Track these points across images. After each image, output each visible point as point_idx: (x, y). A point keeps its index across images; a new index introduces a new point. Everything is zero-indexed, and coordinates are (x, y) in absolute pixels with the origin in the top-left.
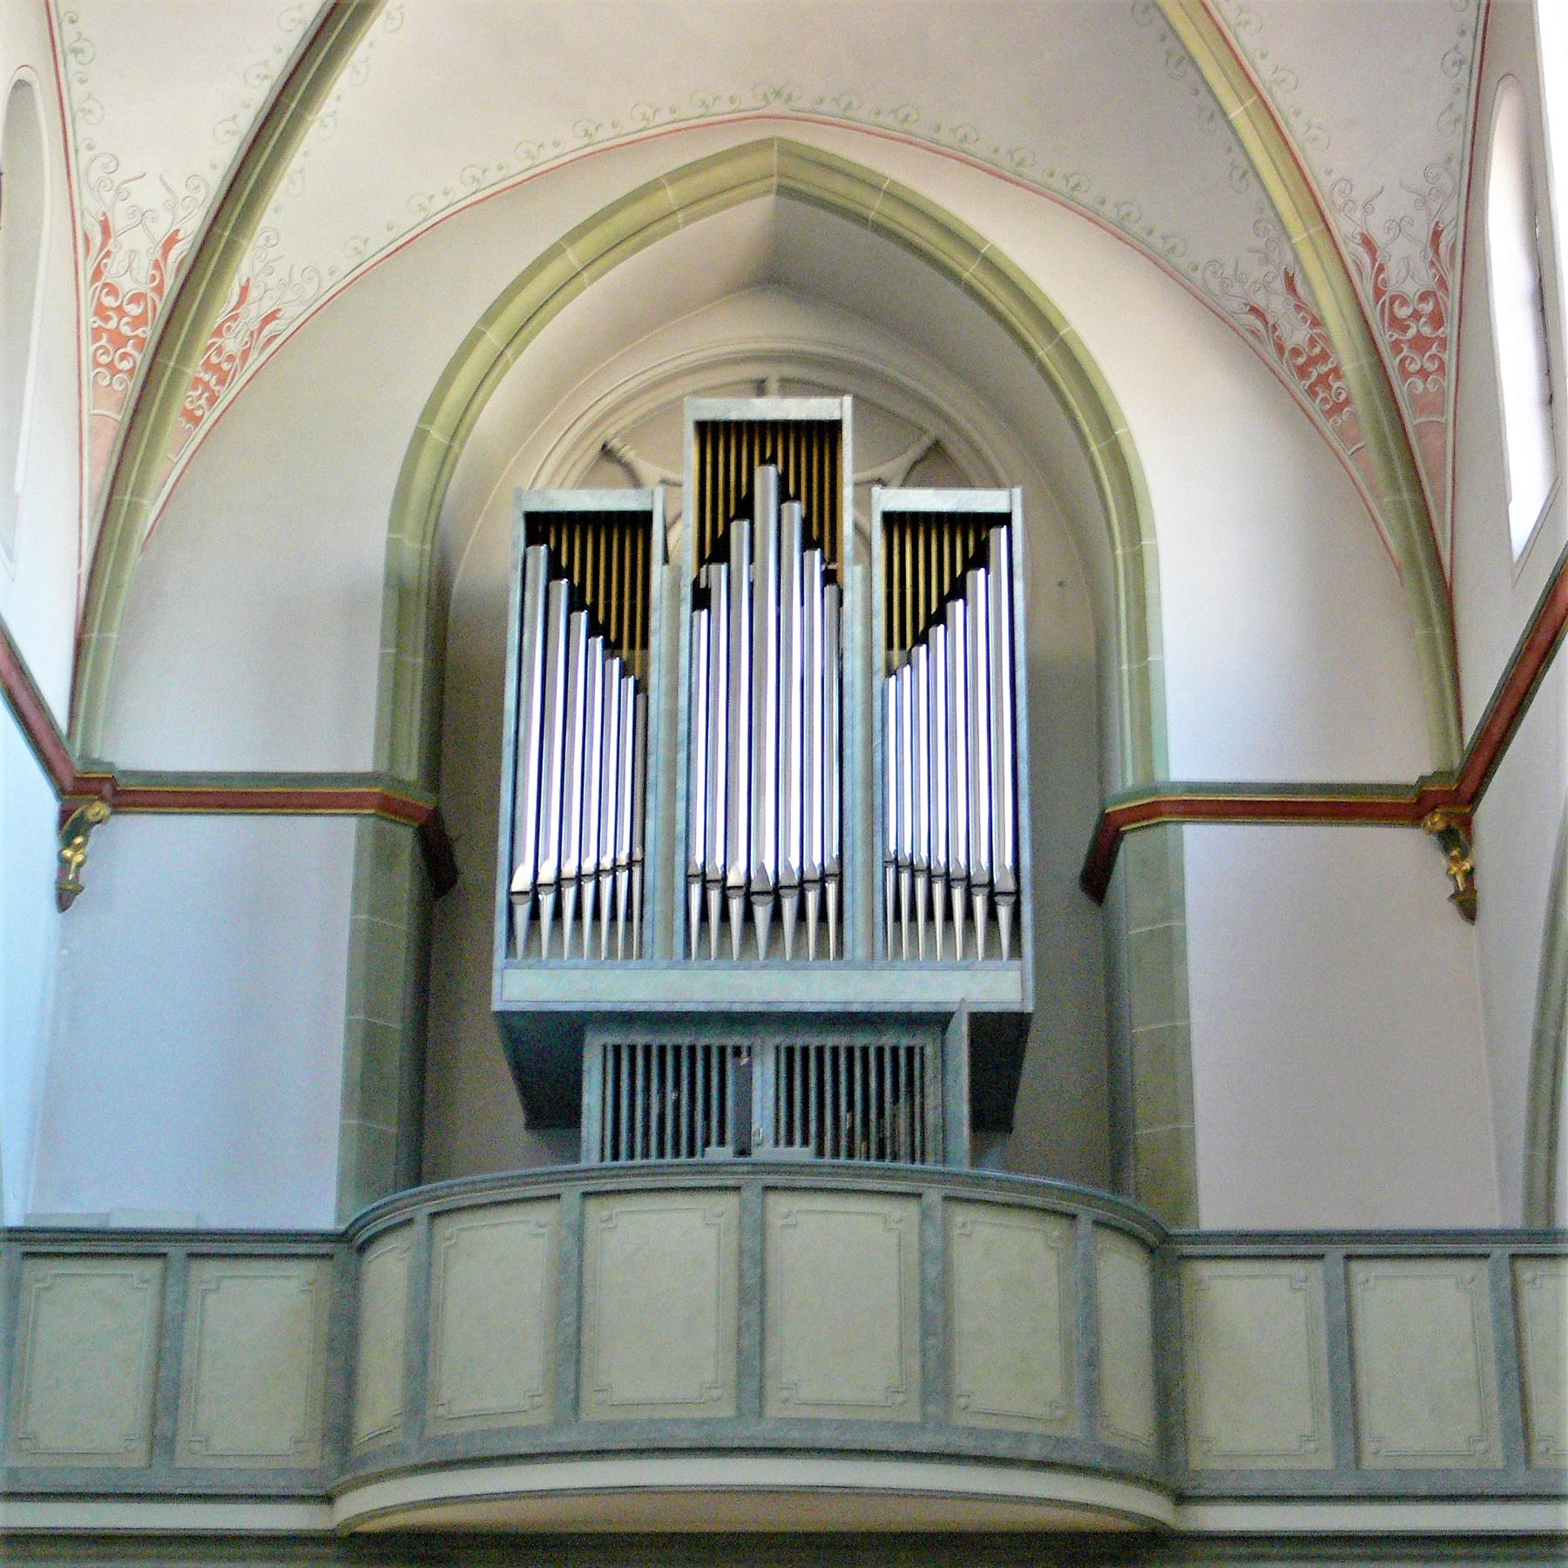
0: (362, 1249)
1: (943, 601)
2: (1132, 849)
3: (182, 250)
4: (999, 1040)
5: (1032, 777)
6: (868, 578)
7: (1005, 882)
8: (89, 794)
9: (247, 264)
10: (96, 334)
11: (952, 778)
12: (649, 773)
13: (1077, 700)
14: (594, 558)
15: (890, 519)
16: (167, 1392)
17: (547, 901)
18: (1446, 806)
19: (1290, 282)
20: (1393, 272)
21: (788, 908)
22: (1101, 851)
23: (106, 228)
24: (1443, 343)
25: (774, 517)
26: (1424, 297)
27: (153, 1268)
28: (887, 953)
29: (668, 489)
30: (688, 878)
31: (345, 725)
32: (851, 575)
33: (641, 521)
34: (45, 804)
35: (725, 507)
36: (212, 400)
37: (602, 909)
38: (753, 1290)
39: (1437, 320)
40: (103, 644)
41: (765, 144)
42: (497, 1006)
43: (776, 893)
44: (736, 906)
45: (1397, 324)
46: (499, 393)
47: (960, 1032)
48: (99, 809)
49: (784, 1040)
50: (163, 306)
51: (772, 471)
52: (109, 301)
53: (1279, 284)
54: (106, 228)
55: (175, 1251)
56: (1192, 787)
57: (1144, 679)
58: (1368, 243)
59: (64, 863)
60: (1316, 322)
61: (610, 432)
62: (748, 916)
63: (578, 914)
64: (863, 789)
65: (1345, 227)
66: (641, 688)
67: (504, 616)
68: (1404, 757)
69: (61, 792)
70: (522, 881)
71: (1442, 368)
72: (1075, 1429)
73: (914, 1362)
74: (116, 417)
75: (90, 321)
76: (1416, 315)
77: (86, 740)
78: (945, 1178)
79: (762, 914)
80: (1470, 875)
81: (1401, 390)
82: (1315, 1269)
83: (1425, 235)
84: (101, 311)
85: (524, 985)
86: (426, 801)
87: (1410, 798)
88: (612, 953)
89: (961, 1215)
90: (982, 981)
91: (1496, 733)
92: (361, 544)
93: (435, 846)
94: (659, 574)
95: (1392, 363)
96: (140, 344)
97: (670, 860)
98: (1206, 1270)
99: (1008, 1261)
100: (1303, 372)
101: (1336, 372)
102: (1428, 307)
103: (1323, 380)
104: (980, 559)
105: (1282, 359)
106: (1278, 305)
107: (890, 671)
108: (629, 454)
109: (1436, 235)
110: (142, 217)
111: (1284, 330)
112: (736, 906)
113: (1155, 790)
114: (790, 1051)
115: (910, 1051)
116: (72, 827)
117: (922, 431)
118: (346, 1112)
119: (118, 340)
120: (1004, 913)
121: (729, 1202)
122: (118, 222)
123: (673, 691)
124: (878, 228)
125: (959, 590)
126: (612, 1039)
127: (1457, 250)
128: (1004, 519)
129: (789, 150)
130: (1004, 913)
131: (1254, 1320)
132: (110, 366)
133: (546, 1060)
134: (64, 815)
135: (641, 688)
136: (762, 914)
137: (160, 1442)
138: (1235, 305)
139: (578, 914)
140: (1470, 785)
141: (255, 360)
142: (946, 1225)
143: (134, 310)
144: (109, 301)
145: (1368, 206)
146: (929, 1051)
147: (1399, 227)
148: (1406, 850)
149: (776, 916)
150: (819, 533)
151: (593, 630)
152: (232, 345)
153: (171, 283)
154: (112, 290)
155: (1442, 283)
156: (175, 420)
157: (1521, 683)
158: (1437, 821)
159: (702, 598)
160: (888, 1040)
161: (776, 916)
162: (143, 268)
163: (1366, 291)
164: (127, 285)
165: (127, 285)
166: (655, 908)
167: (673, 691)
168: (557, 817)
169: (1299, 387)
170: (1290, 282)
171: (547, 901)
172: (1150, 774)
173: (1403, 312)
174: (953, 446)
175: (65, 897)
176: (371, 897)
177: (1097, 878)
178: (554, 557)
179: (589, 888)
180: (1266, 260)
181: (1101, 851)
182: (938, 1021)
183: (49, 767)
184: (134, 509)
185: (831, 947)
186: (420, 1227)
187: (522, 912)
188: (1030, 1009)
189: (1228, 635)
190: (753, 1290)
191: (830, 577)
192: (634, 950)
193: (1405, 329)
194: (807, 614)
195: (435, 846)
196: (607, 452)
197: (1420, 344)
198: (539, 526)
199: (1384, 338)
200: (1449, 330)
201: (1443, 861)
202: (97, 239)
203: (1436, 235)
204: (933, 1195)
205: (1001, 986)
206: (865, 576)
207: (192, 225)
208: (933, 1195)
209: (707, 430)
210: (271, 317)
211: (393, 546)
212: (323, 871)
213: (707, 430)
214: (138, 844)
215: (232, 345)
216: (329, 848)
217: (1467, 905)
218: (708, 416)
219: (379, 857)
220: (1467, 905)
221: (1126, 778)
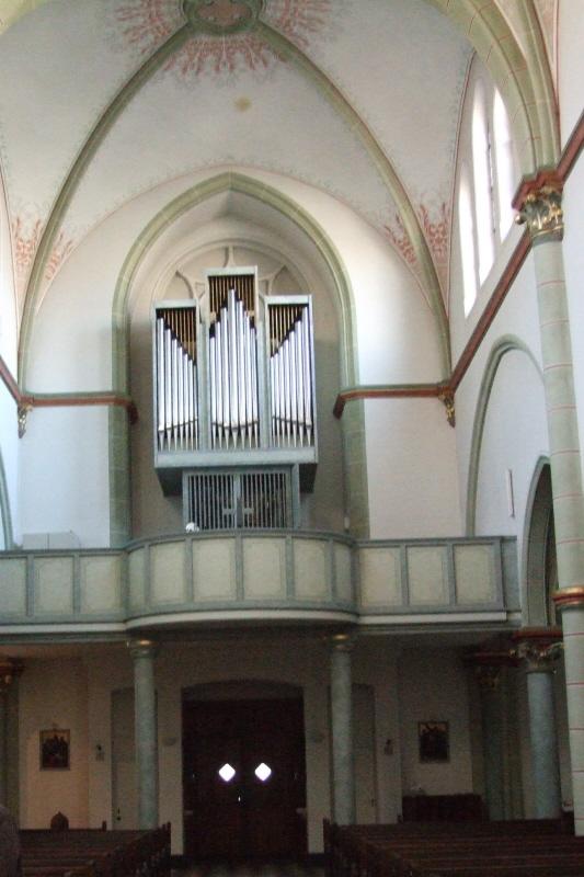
0: (129, 553)
1: (288, 332)
2: (347, 407)
3: (42, 225)
4: (308, 471)
5: (317, 391)
6: (264, 326)
7: (308, 422)
8: (26, 402)
9: (63, 227)
10: (17, 255)
11: (291, 384)
12: (200, 390)
13: (330, 356)
14: (180, 322)
15: (270, 306)
16: (77, 594)
17: (169, 433)
18: (446, 391)
19: (398, 219)
20: (431, 216)
21: (244, 433)
22: (338, 404)
23: (18, 221)
24: (446, 241)
25: (235, 309)
26: (440, 225)
27: (70, 560)
28: (273, 445)
29: (202, 303)
30: (212, 424)
31: (100, 376)
32: (259, 325)
33: (192, 310)
34: (13, 406)
35: (219, 303)
36: (54, 271)
37: (187, 434)
38: (240, 564)
39: (444, 233)
40: (26, 354)
41: (226, 175)
42: (156, 466)
43: (239, 428)
44: (227, 432)
45: (432, 234)
46: (142, 266)
47: (296, 470)
48: (29, 407)
49: (242, 473)
50: (37, 244)
51: (233, 292)
52: (20, 243)
53: (394, 219)
54: (18, 221)
55: (76, 555)
56: (367, 387)
57: (351, 351)
58: (422, 207)
59: (20, 424)
60: (406, 232)
61: (179, 267)
62: (231, 434)
63: (179, 436)
64: (264, 392)
65: (415, 202)
66: (195, 363)
67: (151, 346)
68: (433, 375)
69: (17, 402)
70: (161, 428)
71: (446, 249)
72: (329, 599)
73: (285, 583)
74: (24, 280)
75: (15, 251)
76: (437, 231)
77: (24, 385)
78: (293, 532)
79: (235, 435)
80: (453, 413)
81: (433, 256)
82: (398, 550)
83: (440, 204)
84: (18, 247)
85: (165, 459)
86: (127, 398)
87: (435, 389)
88: (189, 447)
89: (297, 542)
90: (301, 453)
91: (500, 293)
92: (103, 317)
93: (131, 407)
94: (199, 327)
95: (430, 246)
96: (30, 256)
97: (206, 419)
98: (366, 551)
99: (309, 555)
100: (402, 248)
101: (412, 249)
102: (441, 229)
103: (408, 251)
104: (299, 317)
105: (395, 245)
106: (393, 225)
107: (272, 355)
108: (185, 275)
109: (444, 206)
110: (29, 216)
111: (396, 234)
112: (227, 432)
113: (355, 389)
114: (245, 477)
115: (281, 475)
116: (21, 413)
117: (279, 263)
118: (111, 497)
119: (24, 255)
120: (309, 432)
121: (233, 540)
122: (22, 218)
123: (205, 364)
124: (264, 202)
125: (293, 328)
126: (191, 474)
127: (450, 211)
128: (307, 305)
129: (234, 176)
130: (309, 432)
131: (380, 569)
132: (23, 265)
133: (171, 481)
134: (19, 409)
135: (195, 363)
136: (235, 435)
137: (76, 607)
138: (379, 225)
139: (179, 436)
140: (561, 172)
141: (65, 257)
142: (293, 545)
143: (28, 245)
144: (20, 243)
145: (422, 195)
146: (287, 475)
147: (432, 202)
148: (433, 405)
149: (239, 434)
150: (249, 306)
151: (173, 337)
152: (59, 253)
153: (39, 237)
154: (21, 240)
155: (446, 221)
156: (44, 279)
157: (467, 359)
158: (443, 397)
159: (212, 333)
160: (274, 472)
161: (239, 434)
162: (30, 232)
163: (422, 223)
164: (26, 238)
165: (26, 238)
166: (202, 435)
167: (205, 364)
168: (172, 407)
169: (401, 253)
170: (398, 219)
171: (169, 433)
172: (354, 382)
173: (433, 230)
174: (290, 267)
175: (21, 433)
176: (113, 428)
177: (338, 411)
178: (166, 322)
179: (181, 428)
180: (389, 211)
181: (338, 404)
182: (290, 466)
183: (15, 397)
184: (33, 310)
185: (256, 445)
186: (146, 547)
187: (162, 437)
188: (317, 461)
189: (378, 330)
190: (240, 564)
191: (252, 325)
192: (197, 447)
193: (434, 235)
194: (246, 337)
195: (131, 407)
196: (178, 274)
197: (439, 241)
198: (160, 313)
199: (427, 239)
200: (448, 236)
201: (444, 408)
202: (16, 224)
203: (444, 206)
204: (289, 537)
205: (307, 455)
206: (263, 327)
207: (45, 217)
208: (289, 537)
209: (212, 279)
210: (70, 243)
211: (114, 317)
212: (98, 419)
213: (212, 279)
214: (39, 415)
215: (59, 253)
216: (99, 416)
217: (452, 422)
218: (211, 274)
219: (114, 418)
220: (452, 422)
221: (346, 384)
